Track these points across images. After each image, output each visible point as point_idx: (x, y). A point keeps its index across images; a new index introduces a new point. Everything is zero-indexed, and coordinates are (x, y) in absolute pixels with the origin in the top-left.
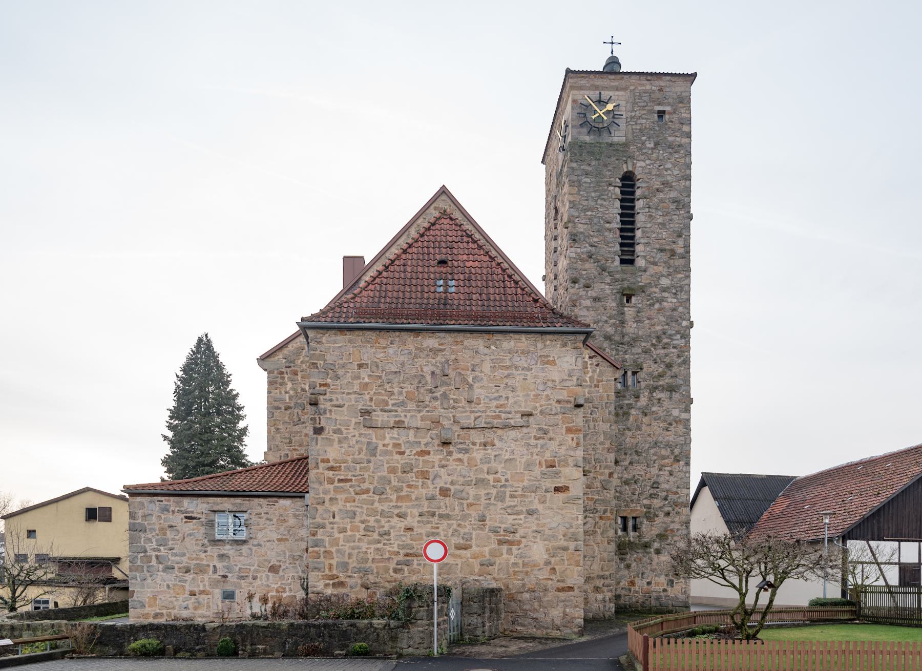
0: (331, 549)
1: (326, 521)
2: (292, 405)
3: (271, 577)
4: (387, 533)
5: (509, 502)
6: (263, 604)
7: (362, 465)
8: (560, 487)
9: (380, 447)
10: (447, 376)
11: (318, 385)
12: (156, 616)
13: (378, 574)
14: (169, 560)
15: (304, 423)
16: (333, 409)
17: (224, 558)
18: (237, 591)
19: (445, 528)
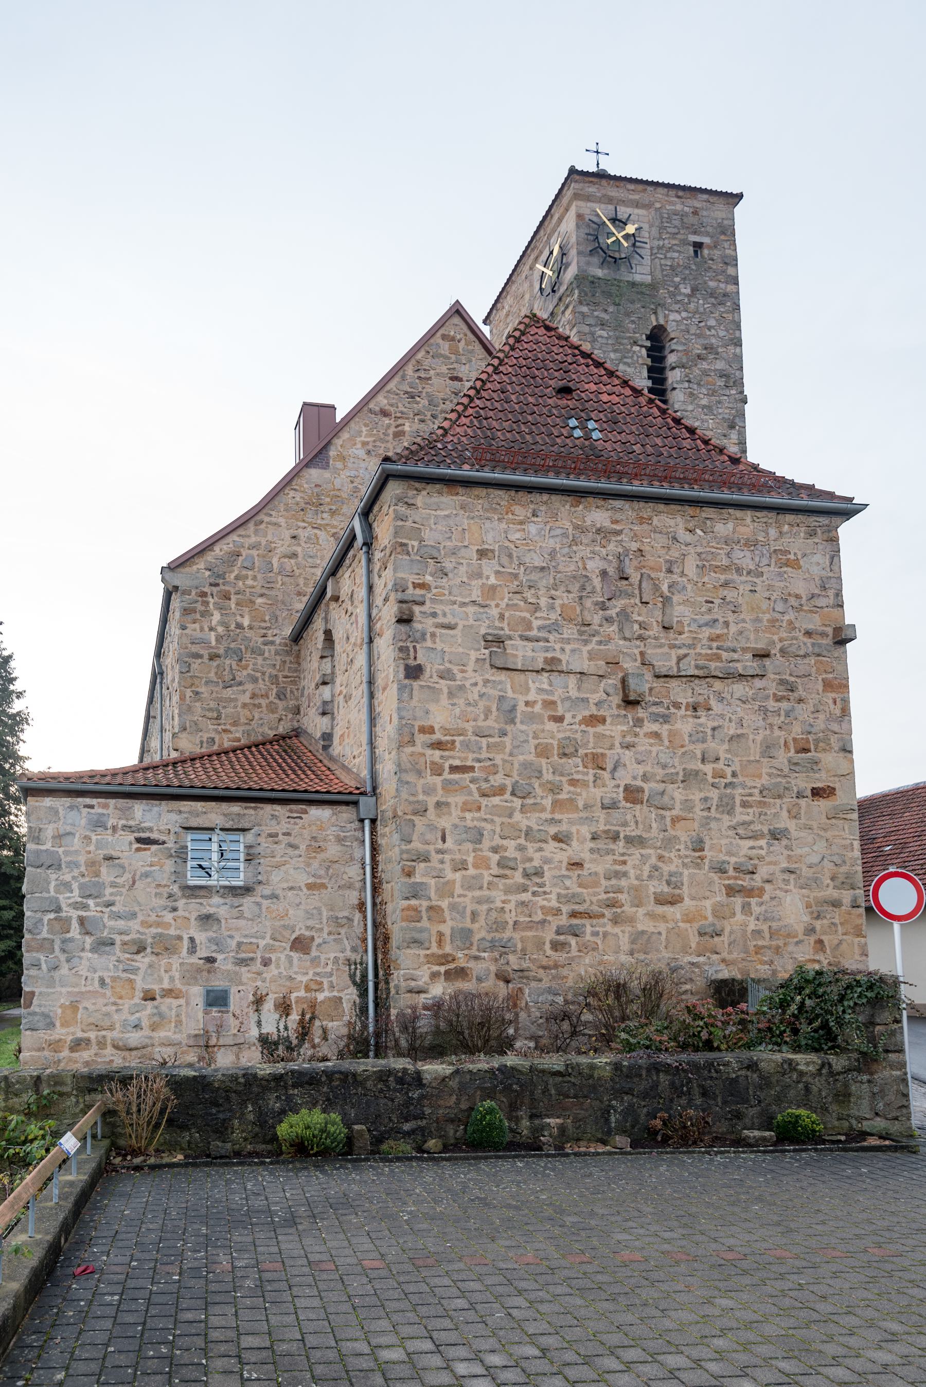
0: (439, 903)
1: (431, 848)
2: (221, 651)
3: (295, 961)
4: (539, 873)
5: (741, 815)
6: (281, 1016)
7: (490, 740)
8: (823, 789)
9: (521, 707)
10: (627, 579)
11: (410, 586)
12: (78, 1044)
13: (524, 952)
14: (104, 926)
15: (240, 684)
16: (439, 631)
17: (210, 921)
18: (233, 990)
19: (637, 862)
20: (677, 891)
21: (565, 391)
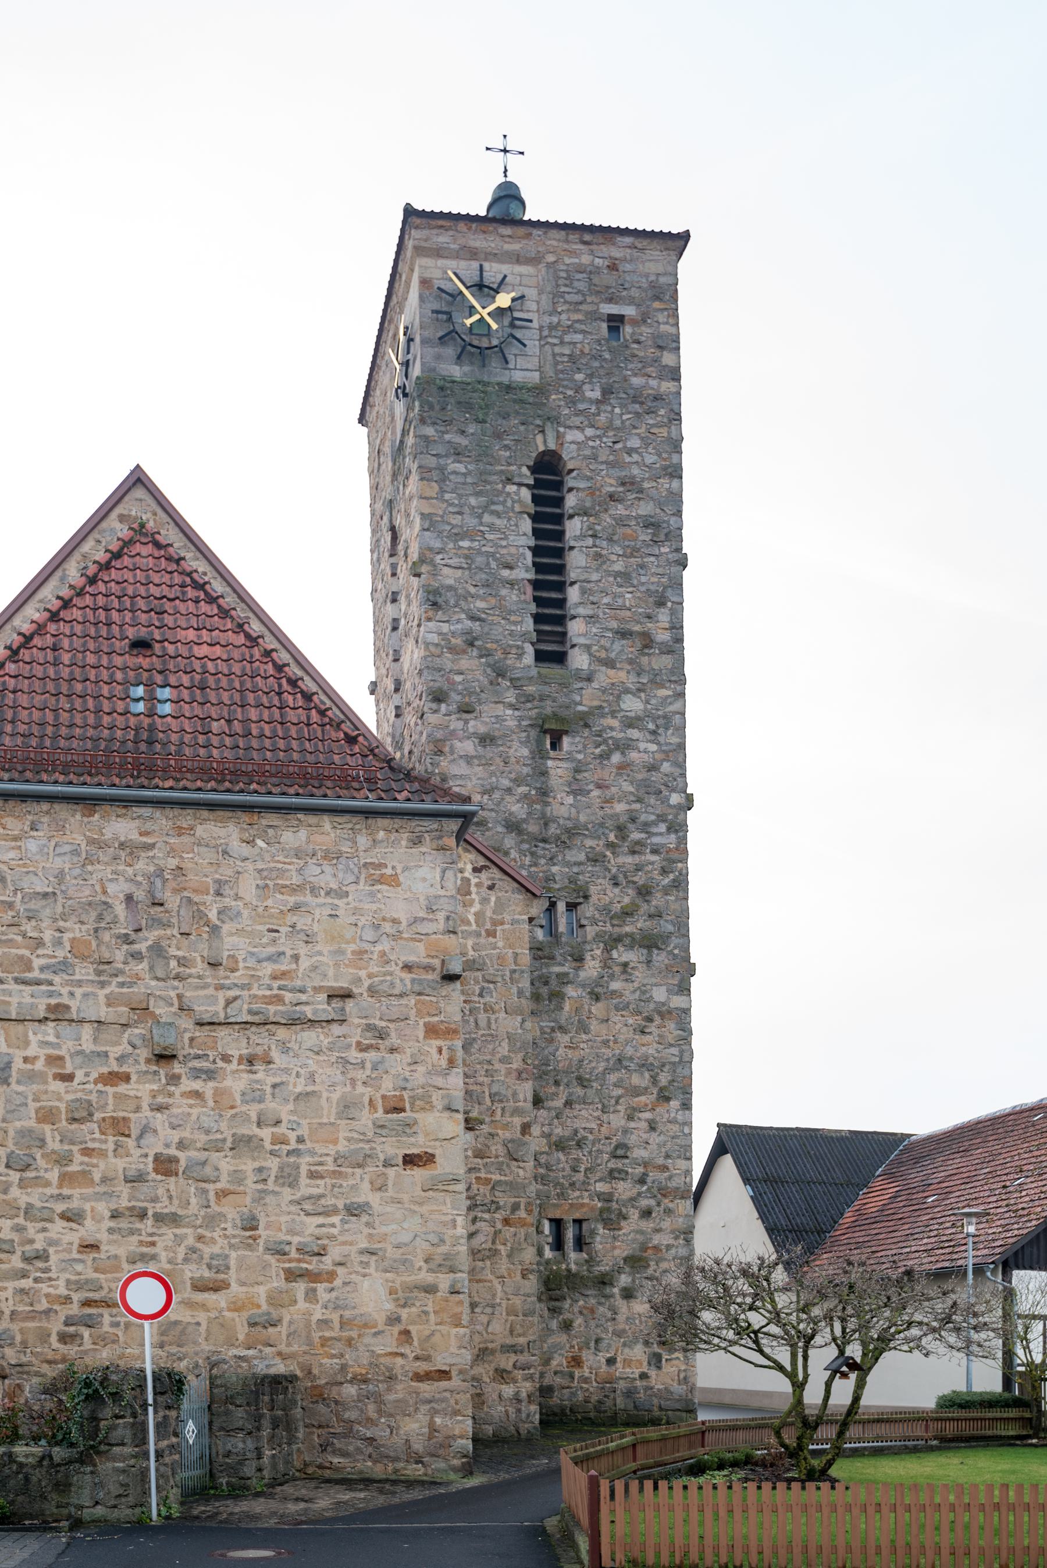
4: (42, 1256)
5: (306, 1187)
8: (418, 1156)
9: (18, 1064)
10: (162, 905)
13: (24, 1344)
19: (170, 1244)
20: (222, 1276)
21: (141, 645)
